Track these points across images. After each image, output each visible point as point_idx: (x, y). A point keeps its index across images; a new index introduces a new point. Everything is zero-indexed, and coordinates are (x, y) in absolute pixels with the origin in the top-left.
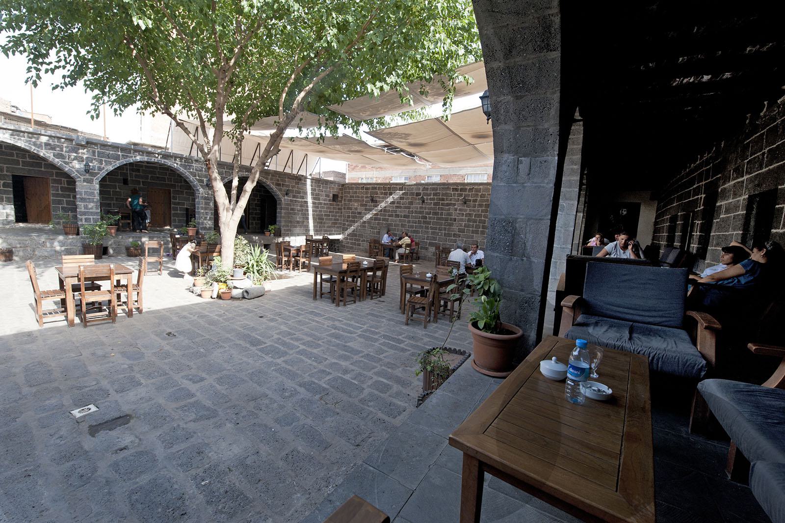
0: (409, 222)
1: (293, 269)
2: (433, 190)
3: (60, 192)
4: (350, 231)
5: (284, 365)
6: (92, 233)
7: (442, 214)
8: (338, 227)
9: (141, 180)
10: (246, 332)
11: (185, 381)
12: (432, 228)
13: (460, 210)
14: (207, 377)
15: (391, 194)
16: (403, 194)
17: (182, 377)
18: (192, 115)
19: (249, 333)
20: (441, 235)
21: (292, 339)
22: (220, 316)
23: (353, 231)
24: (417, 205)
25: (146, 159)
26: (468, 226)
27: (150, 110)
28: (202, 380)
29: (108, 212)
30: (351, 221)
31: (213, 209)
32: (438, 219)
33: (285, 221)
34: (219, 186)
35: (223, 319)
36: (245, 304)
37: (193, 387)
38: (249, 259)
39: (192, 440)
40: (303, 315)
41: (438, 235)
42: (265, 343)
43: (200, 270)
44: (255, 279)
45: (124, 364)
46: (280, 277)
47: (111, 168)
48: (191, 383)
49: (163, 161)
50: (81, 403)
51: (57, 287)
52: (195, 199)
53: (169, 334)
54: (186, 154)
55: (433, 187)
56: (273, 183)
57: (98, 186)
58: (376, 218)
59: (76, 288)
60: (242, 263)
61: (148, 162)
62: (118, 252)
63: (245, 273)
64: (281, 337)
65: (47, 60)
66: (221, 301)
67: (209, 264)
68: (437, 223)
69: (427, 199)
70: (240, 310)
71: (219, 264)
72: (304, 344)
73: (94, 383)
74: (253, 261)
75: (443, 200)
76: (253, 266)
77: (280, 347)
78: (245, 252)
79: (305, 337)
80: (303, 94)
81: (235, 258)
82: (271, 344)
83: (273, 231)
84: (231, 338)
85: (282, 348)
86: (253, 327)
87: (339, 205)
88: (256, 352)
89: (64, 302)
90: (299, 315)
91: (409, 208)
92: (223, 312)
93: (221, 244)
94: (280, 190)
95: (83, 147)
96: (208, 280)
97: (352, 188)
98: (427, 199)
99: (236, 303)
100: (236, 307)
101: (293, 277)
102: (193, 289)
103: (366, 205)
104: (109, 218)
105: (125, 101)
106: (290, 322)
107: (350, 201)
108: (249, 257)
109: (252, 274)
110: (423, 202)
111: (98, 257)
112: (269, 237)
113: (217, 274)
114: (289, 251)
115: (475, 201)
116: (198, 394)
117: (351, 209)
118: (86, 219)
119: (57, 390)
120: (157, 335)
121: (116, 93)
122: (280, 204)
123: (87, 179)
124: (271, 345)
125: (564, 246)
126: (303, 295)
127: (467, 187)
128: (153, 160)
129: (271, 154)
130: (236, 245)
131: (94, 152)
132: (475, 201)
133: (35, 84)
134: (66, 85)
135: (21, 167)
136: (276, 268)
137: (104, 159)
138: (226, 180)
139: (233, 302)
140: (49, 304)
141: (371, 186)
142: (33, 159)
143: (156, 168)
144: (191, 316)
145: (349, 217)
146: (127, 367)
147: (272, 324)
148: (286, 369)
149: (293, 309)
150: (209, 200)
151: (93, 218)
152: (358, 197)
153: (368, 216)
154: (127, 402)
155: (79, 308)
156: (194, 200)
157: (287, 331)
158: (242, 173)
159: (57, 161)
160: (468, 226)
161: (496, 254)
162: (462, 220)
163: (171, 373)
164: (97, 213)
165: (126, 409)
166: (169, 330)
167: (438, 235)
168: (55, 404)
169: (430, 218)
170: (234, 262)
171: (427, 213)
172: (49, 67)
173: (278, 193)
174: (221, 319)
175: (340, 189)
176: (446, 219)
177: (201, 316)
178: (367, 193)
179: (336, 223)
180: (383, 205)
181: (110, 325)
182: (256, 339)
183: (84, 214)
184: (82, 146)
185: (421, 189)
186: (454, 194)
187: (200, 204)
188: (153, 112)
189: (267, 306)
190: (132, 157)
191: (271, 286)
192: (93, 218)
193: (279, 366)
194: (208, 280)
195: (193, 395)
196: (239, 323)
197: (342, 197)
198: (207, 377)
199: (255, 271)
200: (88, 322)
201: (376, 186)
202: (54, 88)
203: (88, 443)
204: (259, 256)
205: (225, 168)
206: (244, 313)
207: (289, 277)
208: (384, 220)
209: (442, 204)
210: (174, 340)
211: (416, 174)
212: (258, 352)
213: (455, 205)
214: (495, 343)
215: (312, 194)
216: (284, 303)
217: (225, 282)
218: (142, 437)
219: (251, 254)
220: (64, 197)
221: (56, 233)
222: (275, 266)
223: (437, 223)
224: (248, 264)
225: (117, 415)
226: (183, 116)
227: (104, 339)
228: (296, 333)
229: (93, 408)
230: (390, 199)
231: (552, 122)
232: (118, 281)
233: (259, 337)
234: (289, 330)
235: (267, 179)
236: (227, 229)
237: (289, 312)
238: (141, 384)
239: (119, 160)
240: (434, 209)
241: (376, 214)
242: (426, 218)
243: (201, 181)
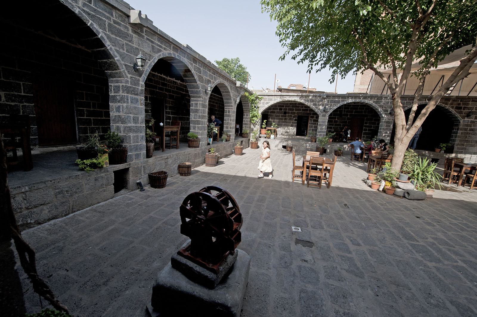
1: (463, 184)
5: (434, 270)
6: (321, 141)
10: (401, 225)
11: (347, 240)
14: (363, 244)
17: (347, 236)
18: (388, 66)
19: (404, 227)
21: (449, 250)
22: (382, 205)
25: (354, 100)
27: (360, 71)
28: (359, 245)
29: (330, 131)
31: (392, 130)
33: (460, 141)
34: (400, 113)
35: (383, 208)
36: (404, 202)
37: (352, 247)
38: (416, 168)
39: (342, 283)
40: (468, 231)
42: (418, 241)
43: (374, 170)
44: (418, 185)
45: (319, 213)
46: (445, 189)
47: (335, 108)
48: (351, 243)
50: (297, 225)
51: (301, 165)
52: (379, 123)
53: (345, 205)
54: (379, 94)
56: (452, 107)
59: (308, 167)
60: (408, 170)
61: (354, 103)
63: (409, 179)
64: (436, 242)
65: (316, 59)
66: (384, 194)
67: (381, 167)
70: (399, 205)
71: (389, 167)
72: (464, 261)
73: (304, 217)
74: (419, 170)
76: (418, 174)
77: (434, 252)
78: (413, 162)
79: (466, 254)
81: (402, 165)
82: (424, 244)
84: (387, 224)
85: (436, 254)
86: (408, 223)
88: (407, 245)
89: (302, 173)
90: (463, 230)
92: (385, 203)
93: (393, 154)
94: (460, 113)
96: (378, 177)
99: (397, 199)
100: (397, 202)
101: (461, 192)
102: (366, 181)
104: (330, 134)
105: (347, 69)
106: (450, 233)
108: (416, 166)
109: (416, 181)
111: (321, 154)
112: (439, 153)
113: (385, 175)
114: (461, 167)
116: (354, 253)
119: (290, 213)
120: (339, 203)
121: (344, 66)
124: (423, 246)
126: (472, 212)
128: (357, 101)
129: (457, 79)
130: (405, 156)
133: (310, 72)
134: (322, 68)
136: (442, 180)
138: (406, 109)
139: (395, 198)
140: (298, 172)
143: (358, 105)
144: (362, 199)
146: (320, 215)
147: (428, 227)
148: (437, 276)
149: (455, 221)
150: (390, 123)
154: (315, 235)
155: (307, 177)
156: (379, 124)
157: (444, 240)
163: (341, 230)
164: (325, 132)
165: (313, 239)
166: (346, 203)
168: (288, 219)
170: (401, 168)
172: (316, 62)
173: (458, 115)
174: (382, 207)
177: (368, 200)
181: (318, 189)
182: (410, 234)
187: (383, 125)
188: (363, 71)
189: (425, 210)
191: (437, 194)
193: (429, 269)
194: (378, 177)
195: (350, 252)
196: (396, 215)
198: (363, 244)
199: (420, 179)
200: (310, 185)
202: (317, 72)
203: (294, 247)
204: (426, 167)
205: (407, 100)
206: (402, 209)
207: (456, 191)
210: (347, 210)
212: (409, 246)
216: (447, 213)
217: (391, 182)
218: (315, 261)
219: (419, 164)
221: (307, 140)
222: (441, 178)
224: (414, 172)
225: (308, 240)
226: (381, 70)
227: (314, 196)
228: (456, 247)
229: (300, 230)
232: (326, 167)
233: (412, 234)
234: (447, 240)
237: (450, 223)
238: (323, 228)
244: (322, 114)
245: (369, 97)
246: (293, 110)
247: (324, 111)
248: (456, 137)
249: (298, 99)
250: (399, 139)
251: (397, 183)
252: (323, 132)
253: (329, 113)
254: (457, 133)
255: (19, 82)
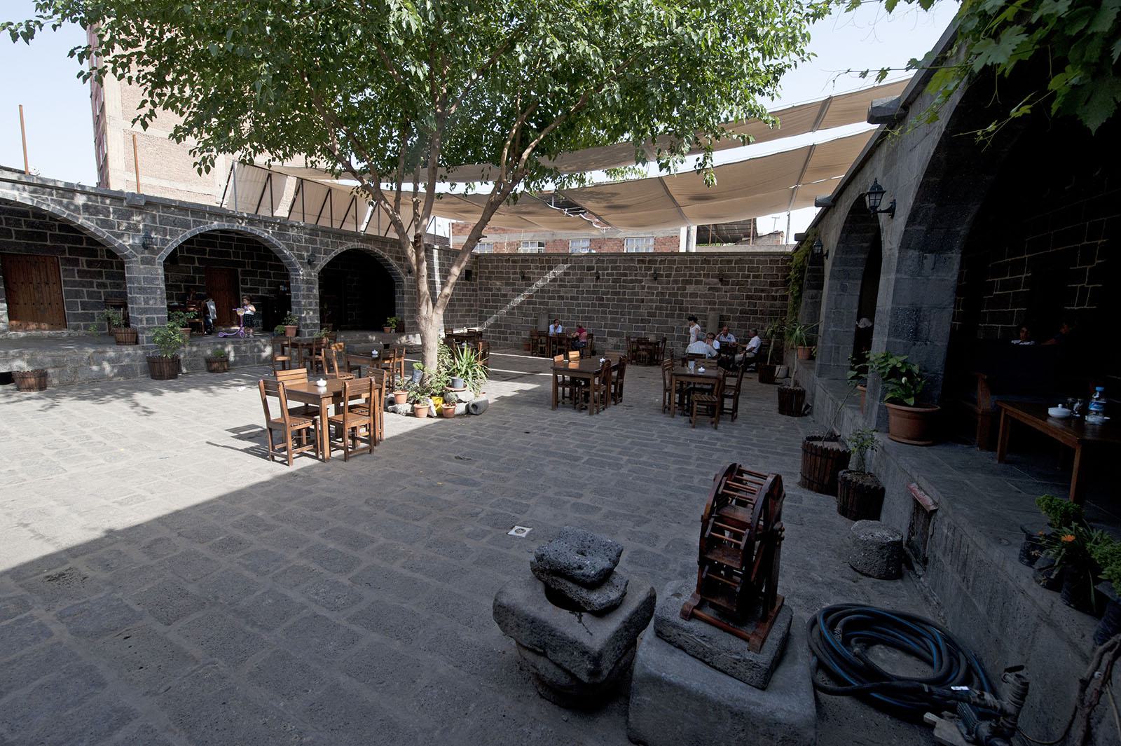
0: (579, 305)
2: (610, 263)
3: (77, 279)
4: (491, 321)
7: (624, 293)
8: (473, 316)
9: (196, 256)
12: (611, 313)
13: (649, 288)
15: (550, 268)
16: (568, 268)
20: (625, 321)
23: (497, 321)
24: (589, 282)
25: (226, 226)
26: (660, 308)
30: (491, 307)
32: (621, 300)
33: (409, 311)
41: (620, 321)
49: (249, 228)
55: (611, 258)
56: (392, 257)
57: (161, 271)
58: (529, 301)
61: (222, 231)
62: (193, 368)
68: (617, 306)
69: (603, 274)
75: (625, 275)
80: (528, 151)
82: (576, 463)
83: (394, 325)
87: (472, 285)
91: (578, 287)
95: (139, 209)
97: (491, 261)
98: (603, 274)
103: (514, 284)
107: (489, 278)
110: (598, 278)
115: (668, 276)
117: (491, 290)
118: (147, 319)
122: (401, 286)
123: (146, 258)
125: (848, 330)
127: (656, 258)
128: (235, 228)
131: (154, 217)
132: (668, 276)
135: (13, 240)
137: (168, 227)
141: (520, 258)
142: (32, 227)
145: (488, 301)
151: (158, 318)
152: (502, 273)
153: (519, 300)
158: (352, 244)
159: (104, 234)
160: (660, 308)
161: (899, 340)
162: (651, 301)
167: (620, 321)
169: (608, 299)
171: (604, 293)
173: (399, 270)
175: (475, 263)
176: (631, 301)
178: (514, 268)
179: (471, 311)
180: (540, 283)
183: (145, 311)
184: (137, 207)
185: (594, 261)
186: (641, 268)
190: (207, 223)
192: (158, 318)
197: (476, 274)
201: (493, 258)
208: (541, 303)
209: (624, 281)
211: (555, 238)
213: (641, 281)
214: (907, 414)
215: (441, 271)
220: (84, 286)
223: (617, 306)
230: (550, 276)
231: (965, 226)
235: (384, 251)
236: (430, 326)
239: (189, 228)
240: (614, 287)
241: (530, 296)
242: (602, 299)
243: (300, 257)
244: (139, 256)
245: (260, 222)
246: (205, 255)
247: (145, 246)
248: (403, 305)
249: (26, 195)
250: (425, 319)
251: (456, 395)
252: (156, 311)
253: (165, 254)
254: (403, 299)
255: (998, 449)
